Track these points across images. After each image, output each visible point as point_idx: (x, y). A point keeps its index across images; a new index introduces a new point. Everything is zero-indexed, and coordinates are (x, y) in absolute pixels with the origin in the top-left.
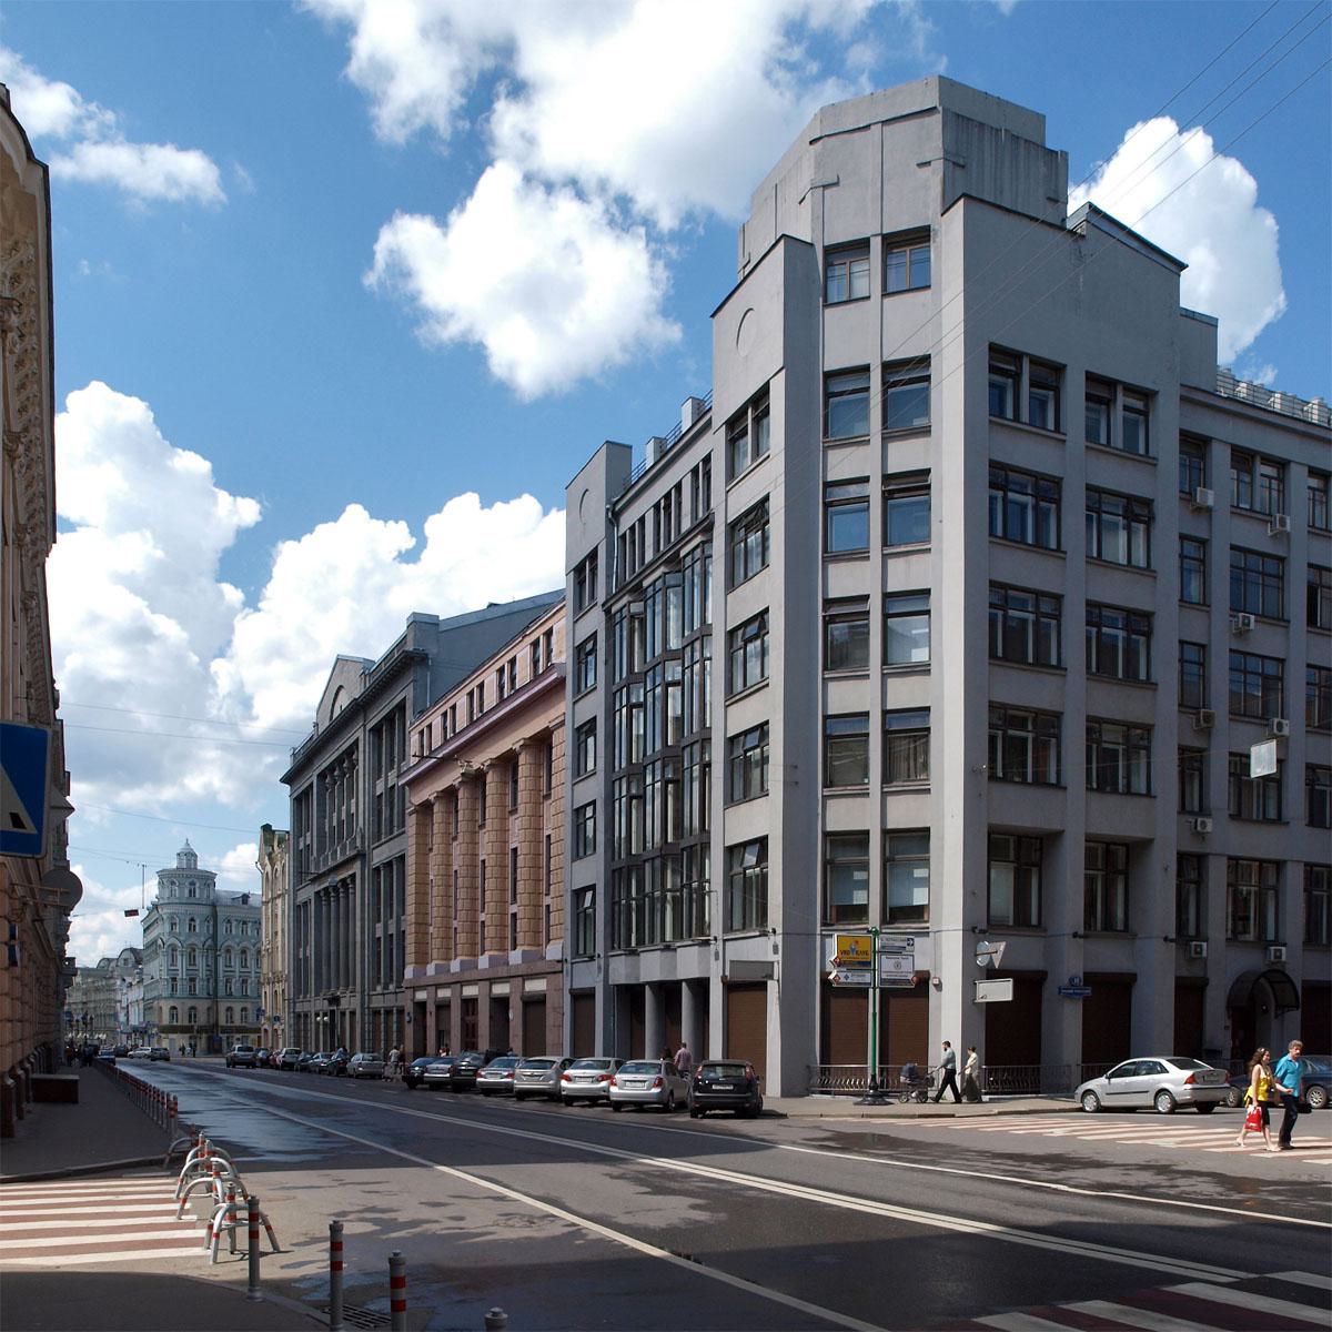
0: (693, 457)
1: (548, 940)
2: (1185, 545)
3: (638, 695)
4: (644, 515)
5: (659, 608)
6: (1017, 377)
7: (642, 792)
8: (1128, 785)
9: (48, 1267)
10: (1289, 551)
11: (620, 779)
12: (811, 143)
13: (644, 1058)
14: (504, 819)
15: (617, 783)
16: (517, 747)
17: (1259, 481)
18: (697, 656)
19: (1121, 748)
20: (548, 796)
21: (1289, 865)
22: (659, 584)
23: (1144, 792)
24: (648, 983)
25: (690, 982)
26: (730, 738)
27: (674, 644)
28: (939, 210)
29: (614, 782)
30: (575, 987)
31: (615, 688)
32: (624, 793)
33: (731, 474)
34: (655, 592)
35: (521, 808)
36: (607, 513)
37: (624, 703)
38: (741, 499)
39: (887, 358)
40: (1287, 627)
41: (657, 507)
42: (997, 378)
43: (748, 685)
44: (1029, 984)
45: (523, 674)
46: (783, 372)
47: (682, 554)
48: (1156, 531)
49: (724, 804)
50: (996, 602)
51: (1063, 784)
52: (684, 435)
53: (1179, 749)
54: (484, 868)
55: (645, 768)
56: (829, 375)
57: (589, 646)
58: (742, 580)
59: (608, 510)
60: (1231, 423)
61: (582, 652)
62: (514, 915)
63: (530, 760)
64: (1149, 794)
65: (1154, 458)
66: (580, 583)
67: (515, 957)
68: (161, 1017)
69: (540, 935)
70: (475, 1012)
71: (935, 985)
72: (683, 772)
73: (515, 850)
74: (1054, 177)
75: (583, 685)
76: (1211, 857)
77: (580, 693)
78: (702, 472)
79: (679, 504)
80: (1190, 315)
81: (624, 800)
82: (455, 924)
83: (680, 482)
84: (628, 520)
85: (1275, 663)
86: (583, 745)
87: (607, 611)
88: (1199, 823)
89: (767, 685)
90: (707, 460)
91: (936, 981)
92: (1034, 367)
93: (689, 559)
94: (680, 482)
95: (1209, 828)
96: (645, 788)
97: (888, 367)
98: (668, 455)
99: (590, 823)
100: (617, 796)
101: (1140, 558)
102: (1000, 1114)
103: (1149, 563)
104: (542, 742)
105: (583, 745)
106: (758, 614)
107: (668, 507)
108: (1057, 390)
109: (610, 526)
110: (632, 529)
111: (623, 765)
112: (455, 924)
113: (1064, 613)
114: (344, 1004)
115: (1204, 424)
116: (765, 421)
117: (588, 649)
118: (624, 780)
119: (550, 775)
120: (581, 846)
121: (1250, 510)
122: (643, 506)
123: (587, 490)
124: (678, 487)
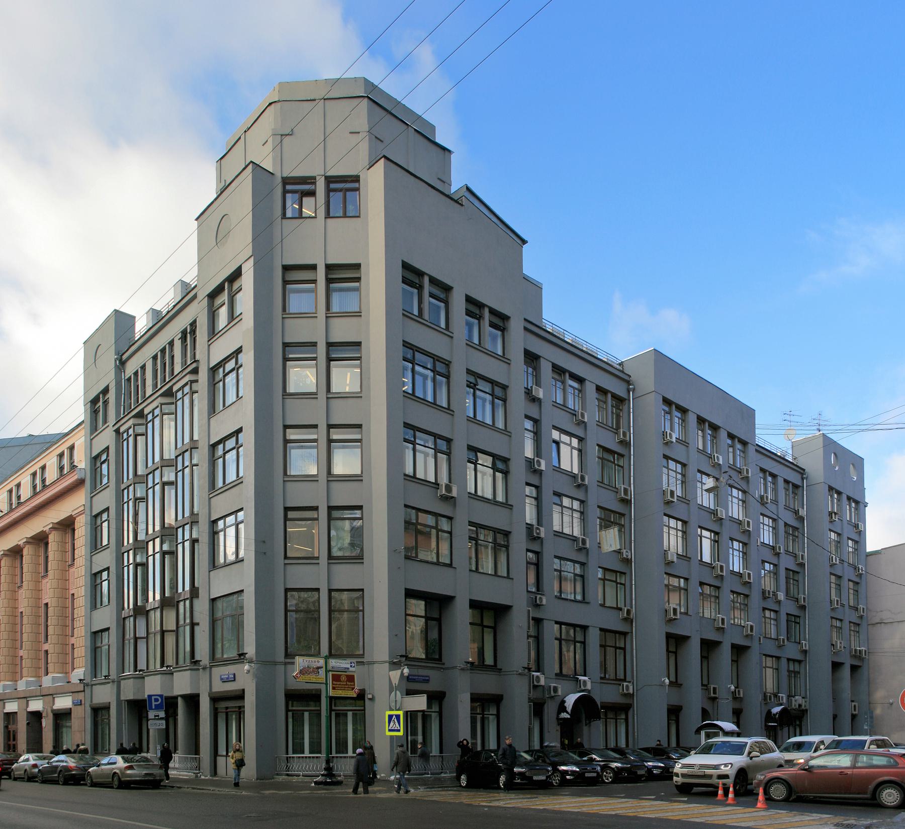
0: (182, 322)
1: (73, 669)
2: (574, 503)
3: (169, 476)
6: (420, 288)
7: (145, 560)
8: (335, 190)
9: (209, 552)
10: (750, 591)
12: (350, 133)
14: (38, 582)
15: (126, 554)
16: (21, 543)
17: (570, 390)
18: (187, 463)
19: (334, 755)
20: (72, 565)
21: (591, 629)
23: (506, 575)
25: (184, 697)
26: (94, 574)
27: (170, 454)
28: (366, 163)
29: (123, 553)
30: (215, 689)
31: (123, 486)
32: (131, 561)
33: (213, 333)
34: (129, 436)
35: (50, 573)
36: (116, 361)
38: (220, 350)
39: (330, 262)
40: (511, 509)
43: (227, 482)
44: (406, 665)
45: (51, 474)
46: (252, 258)
48: (511, 477)
49: (91, 609)
50: (473, 536)
51: (679, 682)
52: (220, 331)
53: (733, 713)
54: (22, 617)
55: (147, 543)
56: (286, 268)
57: (104, 457)
58: (221, 408)
60: (806, 784)
61: (95, 460)
62: (46, 652)
63: (31, 553)
64: (508, 577)
65: (509, 432)
66: (95, 412)
67: (47, 681)
69: (67, 665)
70: (15, 722)
71: (370, 699)
72: (177, 545)
73: (47, 604)
74: (886, 654)
75: (99, 543)
76: (544, 621)
77: (95, 489)
78: (189, 334)
79: (144, 381)
80: (526, 278)
81: (131, 567)
82: (21, 653)
84: (131, 367)
86: (99, 469)
87: (117, 431)
88: (538, 598)
89: (242, 482)
90: (193, 324)
91: (370, 696)
92: (791, 736)
95: (544, 602)
96: (147, 558)
97: (329, 268)
98: (160, 321)
99: (105, 584)
101: (500, 424)
102: (830, 426)
103: (616, 651)
104: (68, 525)
105: (99, 469)
106: (234, 432)
107: (193, 332)
108: (446, 303)
110: (136, 374)
111: (131, 541)
112: (21, 653)
113: (452, 452)
114: (317, 767)
115: (538, 347)
117: (102, 460)
118: (131, 552)
119: (73, 539)
120: (95, 602)
121: (285, 394)
122: (145, 356)
124: (143, 367)
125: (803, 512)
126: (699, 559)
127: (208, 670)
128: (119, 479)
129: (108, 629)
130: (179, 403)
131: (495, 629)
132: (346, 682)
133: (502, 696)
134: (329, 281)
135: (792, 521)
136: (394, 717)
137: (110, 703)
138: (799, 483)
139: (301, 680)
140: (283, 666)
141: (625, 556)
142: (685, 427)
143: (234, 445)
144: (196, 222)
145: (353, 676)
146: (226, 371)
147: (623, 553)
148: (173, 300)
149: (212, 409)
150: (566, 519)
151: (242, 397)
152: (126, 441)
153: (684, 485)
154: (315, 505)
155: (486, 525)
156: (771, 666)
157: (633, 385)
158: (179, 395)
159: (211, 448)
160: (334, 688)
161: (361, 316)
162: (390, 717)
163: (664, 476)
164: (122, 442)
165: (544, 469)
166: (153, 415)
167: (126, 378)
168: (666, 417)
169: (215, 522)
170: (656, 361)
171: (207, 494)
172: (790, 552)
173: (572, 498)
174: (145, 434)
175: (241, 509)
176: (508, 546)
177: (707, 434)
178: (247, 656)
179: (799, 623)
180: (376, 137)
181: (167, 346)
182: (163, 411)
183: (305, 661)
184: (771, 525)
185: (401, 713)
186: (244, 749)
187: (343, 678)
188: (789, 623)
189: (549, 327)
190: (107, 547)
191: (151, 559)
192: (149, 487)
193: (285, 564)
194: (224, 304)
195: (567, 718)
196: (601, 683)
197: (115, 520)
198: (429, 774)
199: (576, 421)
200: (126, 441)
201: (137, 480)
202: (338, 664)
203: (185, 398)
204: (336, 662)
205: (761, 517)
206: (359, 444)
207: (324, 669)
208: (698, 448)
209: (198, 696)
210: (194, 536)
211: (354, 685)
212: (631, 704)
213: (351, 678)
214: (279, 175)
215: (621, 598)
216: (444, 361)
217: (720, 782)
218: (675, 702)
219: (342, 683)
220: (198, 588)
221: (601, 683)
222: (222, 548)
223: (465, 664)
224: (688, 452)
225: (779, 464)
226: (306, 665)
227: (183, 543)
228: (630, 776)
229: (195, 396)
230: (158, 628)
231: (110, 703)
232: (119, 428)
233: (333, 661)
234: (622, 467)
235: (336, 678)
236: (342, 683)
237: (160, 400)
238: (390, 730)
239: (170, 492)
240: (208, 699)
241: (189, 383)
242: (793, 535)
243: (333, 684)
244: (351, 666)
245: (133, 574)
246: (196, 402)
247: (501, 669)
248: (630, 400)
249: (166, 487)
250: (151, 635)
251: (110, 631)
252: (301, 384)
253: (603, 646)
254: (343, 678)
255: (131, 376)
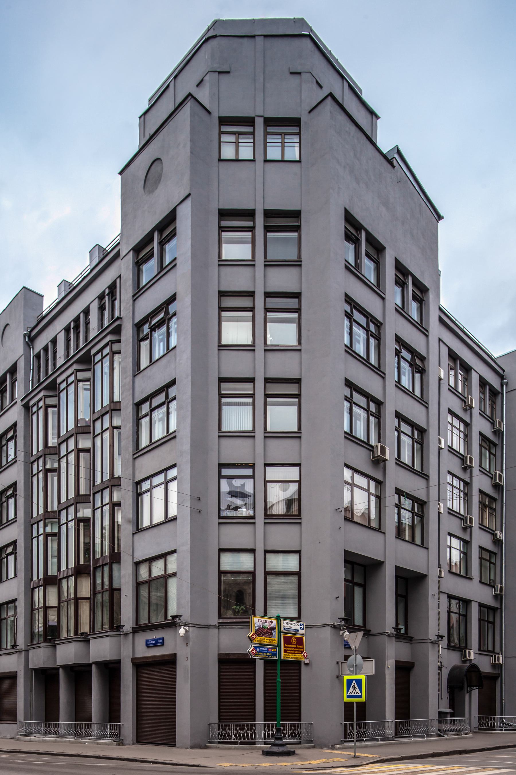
3: (85, 443)
4: (56, 337)
5: (106, 370)
11: (38, 523)
13: (59, 721)
15: (35, 526)
22: (71, 379)
24: (94, 663)
29: (32, 525)
30: (137, 656)
31: (32, 459)
37: (41, 468)
41: (67, 330)
42: (300, 260)
47: (93, 352)
52: (85, 277)
59: (25, 335)
68: (270, 139)
76: (472, 602)
83: (88, 307)
85: (367, 507)
93: (98, 357)
94: (88, 307)
100: (35, 534)
105: (5, 504)
107: (77, 328)
109: (28, 348)
110: (46, 349)
116: (88, 325)
123: (8, 325)
124: (54, 341)
125: (501, 535)
126: (346, 428)
127: (131, 636)
128: (28, 452)
129: (14, 601)
130: (63, 395)
131: (364, 586)
132: (296, 645)
133: (120, 660)
134: (268, 229)
135: (488, 489)
136: (354, 682)
137: (17, 672)
138: (498, 388)
139: (257, 642)
140: (217, 629)
141: (498, 537)
142: (467, 442)
143: (163, 400)
144: (120, 176)
145: (302, 639)
146: (104, 355)
147: (496, 534)
148: (89, 267)
149: (137, 369)
150: (456, 438)
151: (175, 347)
152: (99, 437)
153: (358, 592)
154: (174, 549)
155: (256, 222)
156: (458, 611)
157: (506, 379)
158: (35, 409)
159: (135, 407)
160: (285, 651)
161: (16, 724)
162: (349, 682)
163: (448, 494)
164: (32, 415)
165: (443, 448)
166: (38, 407)
167: (35, 353)
168: (451, 373)
169: (138, 483)
170: (395, 567)
171: (131, 454)
172: (486, 527)
173: (355, 470)
174: (57, 406)
175: (174, 466)
176: (423, 516)
177: (458, 373)
178: (181, 618)
179: (494, 564)
180: (317, 82)
181: (82, 315)
182: (78, 378)
183: (260, 621)
184: (462, 488)
185: (363, 677)
186: (119, 235)
187: (294, 641)
188: (482, 622)
189: (11, 452)
190: (15, 520)
191: (64, 528)
192: (34, 473)
193: (219, 437)
194: (152, 256)
195: (177, 403)
196: (479, 654)
197: (374, 509)
198: (462, 735)
199: (373, 457)
200: (99, 437)
201: (48, 451)
202: (289, 625)
203: (104, 360)
204: (287, 623)
205: (449, 537)
206: (295, 235)
207: (276, 630)
208: (449, 385)
209: (118, 662)
210: (115, 499)
211: (303, 648)
212: (499, 674)
213: (300, 641)
214: (215, 115)
215: (243, 390)
216: (376, 322)
217: (239, 742)
218: (405, 658)
219: (292, 646)
220: (443, 216)
221: (479, 654)
222: (157, 135)
223: (436, 637)
224: (428, 487)
225: (482, 474)
226: (261, 624)
227: (102, 507)
228: (85, 564)
229: (116, 357)
230: (72, 596)
231: (17, 672)
232: (28, 402)
233: (285, 622)
234: (495, 455)
235: (287, 640)
236: (292, 646)
237: (75, 367)
238: (348, 697)
239: (53, 478)
240: (131, 665)
241: (43, 398)
242: (491, 508)
243: (284, 647)
244: (301, 628)
245: (480, 346)
246: (116, 365)
247: (412, 638)
248: (502, 394)
249: (80, 454)
250: (35, 612)
251: (17, 603)
252: (367, 637)
253: (481, 558)
254: (294, 641)
255: (40, 352)
